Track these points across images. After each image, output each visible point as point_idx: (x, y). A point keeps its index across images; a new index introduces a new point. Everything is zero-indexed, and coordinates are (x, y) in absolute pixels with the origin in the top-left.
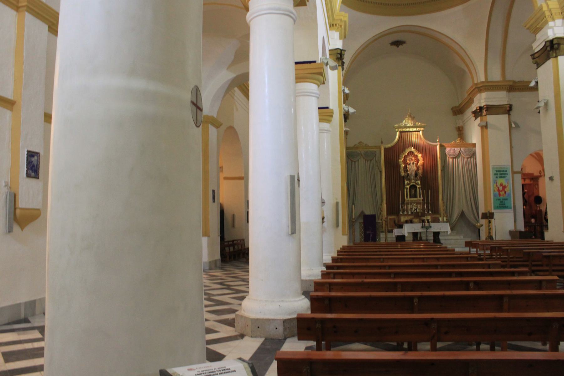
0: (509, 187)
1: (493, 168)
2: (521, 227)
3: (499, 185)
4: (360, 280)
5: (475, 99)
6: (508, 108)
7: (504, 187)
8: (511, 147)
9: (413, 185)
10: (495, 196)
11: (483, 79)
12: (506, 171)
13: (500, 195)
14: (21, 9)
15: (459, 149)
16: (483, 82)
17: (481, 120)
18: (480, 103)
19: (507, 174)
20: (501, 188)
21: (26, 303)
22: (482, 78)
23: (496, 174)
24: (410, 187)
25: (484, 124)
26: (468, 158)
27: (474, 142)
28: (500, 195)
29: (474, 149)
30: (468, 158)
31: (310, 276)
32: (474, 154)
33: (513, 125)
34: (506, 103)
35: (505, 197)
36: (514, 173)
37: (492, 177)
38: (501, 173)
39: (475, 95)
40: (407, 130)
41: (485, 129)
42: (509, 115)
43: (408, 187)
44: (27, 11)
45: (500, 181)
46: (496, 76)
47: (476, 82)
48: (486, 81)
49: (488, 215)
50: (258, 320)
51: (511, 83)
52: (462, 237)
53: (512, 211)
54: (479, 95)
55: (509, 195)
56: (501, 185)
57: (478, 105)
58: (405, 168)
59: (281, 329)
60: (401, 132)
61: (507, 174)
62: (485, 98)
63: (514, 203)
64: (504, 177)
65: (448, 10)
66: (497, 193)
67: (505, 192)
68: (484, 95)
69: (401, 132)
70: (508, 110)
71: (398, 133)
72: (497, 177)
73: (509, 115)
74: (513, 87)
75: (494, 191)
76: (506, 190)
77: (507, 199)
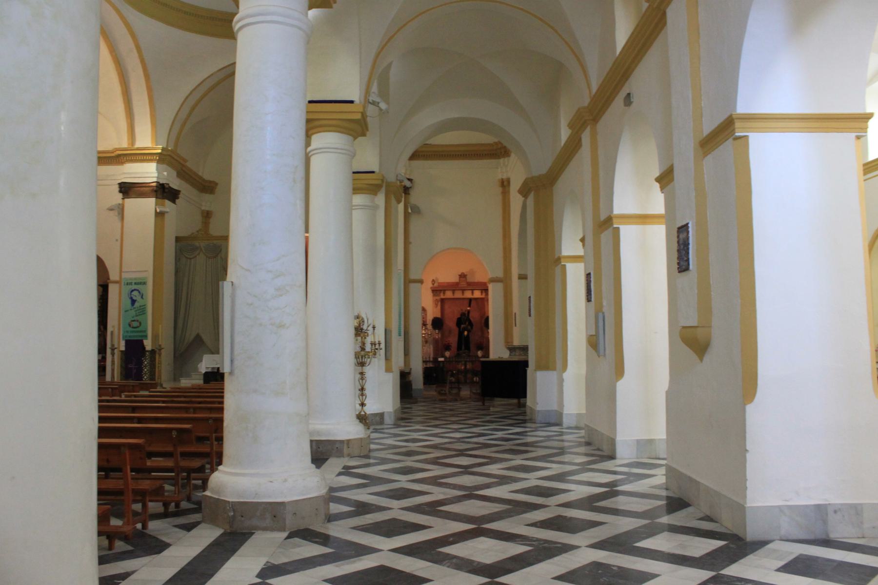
21: (434, 295)
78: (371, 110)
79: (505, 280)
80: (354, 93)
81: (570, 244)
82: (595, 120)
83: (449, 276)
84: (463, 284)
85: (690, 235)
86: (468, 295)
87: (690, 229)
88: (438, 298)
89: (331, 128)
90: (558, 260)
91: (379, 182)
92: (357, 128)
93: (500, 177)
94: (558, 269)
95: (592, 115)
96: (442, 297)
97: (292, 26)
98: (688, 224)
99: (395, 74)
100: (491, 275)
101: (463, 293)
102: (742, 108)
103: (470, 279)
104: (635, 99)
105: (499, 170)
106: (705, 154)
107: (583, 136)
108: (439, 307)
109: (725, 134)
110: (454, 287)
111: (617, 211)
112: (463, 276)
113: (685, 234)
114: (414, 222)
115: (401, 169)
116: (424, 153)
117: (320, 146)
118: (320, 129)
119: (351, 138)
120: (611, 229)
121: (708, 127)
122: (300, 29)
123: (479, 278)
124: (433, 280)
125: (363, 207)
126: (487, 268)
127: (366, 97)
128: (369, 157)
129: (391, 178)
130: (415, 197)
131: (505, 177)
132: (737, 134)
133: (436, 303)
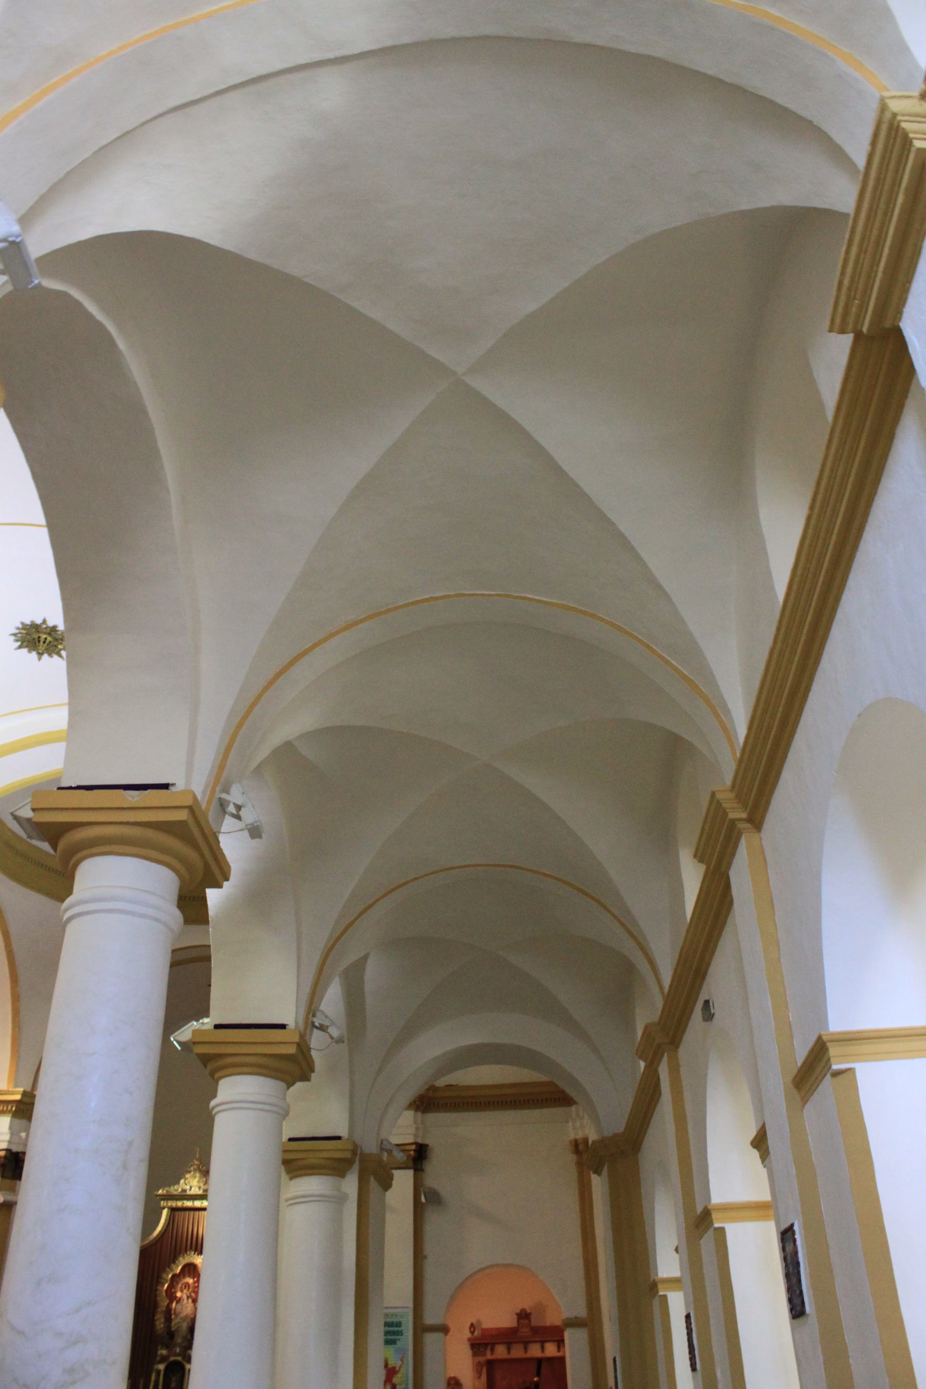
0: (403, 1371)
9: (176, 1363)
12: (399, 1324)
21: (475, 1354)
24: (166, 1369)
40: (189, 1204)
43: (161, 1367)
58: (168, 1312)
60: (173, 1210)
65: (594, 1189)
69: (173, 1210)
71: (165, 1212)
78: (317, 1040)
79: (590, 1322)
80: (286, 1011)
81: (668, 1263)
82: (675, 1041)
83: (499, 1317)
84: (525, 1332)
85: (799, 1243)
86: (535, 1351)
87: (797, 1236)
88: (482, 1359)
89: (245, 1069)
90: (653, 1287)
91: (348, 1155)
92: (293, 1067)
93: (572, 1136)
94: (656, 1302)
95: (668, 1036)
96: (489, 1356)
97: (157, 920)
98: (792, 1225)
99: (374, 975)
100: (567, 1313)
101: (526, 1349)
102: (836, 1024)
103: (535, 1322)
104: (716, 1010)
105: (570, 1124)
106: (805, 1100)
107: (660, 1069)
108: (484, 1377)
109: (816, 1068)
110: (508, 1337)
111: (717, 1198)
112: (523, 1316)
113: (792, 1245)
114: (434, 1222)
115: (403, 1129)
116: (427, 1102)
117: (230, 1098)
118: (231, 1070)
119: (282, 1085)
120: (711, 1232)
121: (801, 1055)
122: (157, 920)
123: (552, 1319)
124: (472, 1325)
125: (321, 1198)
126: (566, 1303)
127: (307, 1018)
128: (322, 1110)
129: (370, 1146)
130: (437, 1174)
131: (580, 1136)
132: (835, 1067)
133: (478, 1368)
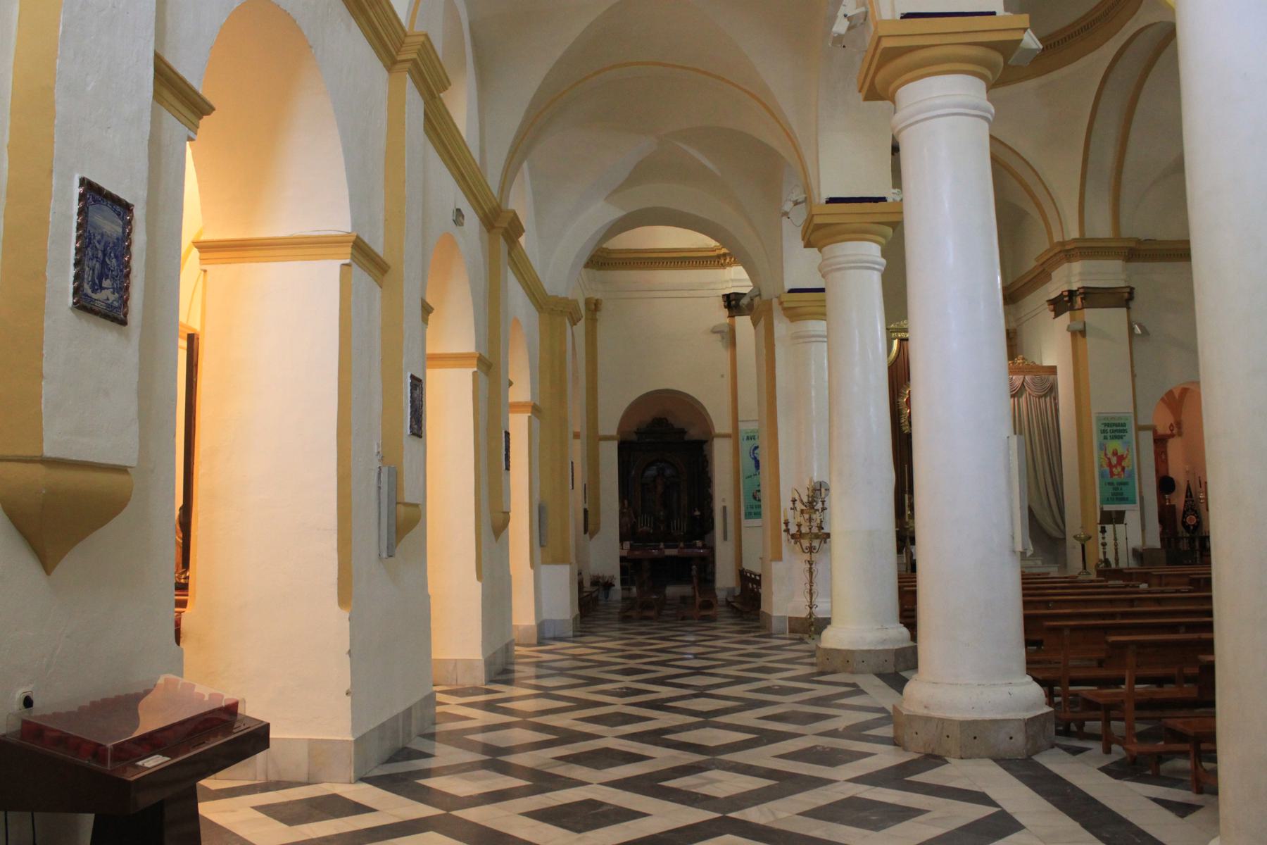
1: (1098, 419)
2: (1154, 541)
3: (1110, 455)
4: (1195, 636)
5: (1053, 274)
6: (1126, 295)
7: (1121, 458)
8: (1134, 376)
10: (1102, 475)
11: (1075, 234)
12: (1124, 425)
13: (1112, 474)
14: (398, 66)
15: (1021, 377)
16: (1075, 240)
17: (1072, 319)
18: (1069, 282)
19: (1125, 431)
20: (1114, 460)
22: (1073, 233)
23: (1103, 431)
25: (1080, 327)
26: (1040, 397)
27: (1048, 362)
28: (1112, 474)
29: (1051, 377)
30: (1040, 397)
31: (884, 641)
32: (1052, 390)
33: (1138, 330)
34: (1122, 284)
35: (1123, 478)
36: (1140, 428)
37: (1096, 438)
38: (1114, 429)
39: (1058, 264)
41: (1079, 336)
42: (1128, 308)
44: (410, 72)
45: (1114, 445)
46: (1101, 228)
47: (1057, 238)
48: (1082, 239)
49: (1114, 516)
50: (975, 722)
51: (1132, 245)
52: (1039, 563)
53: (1137, 507)
54: (1066, 265)
55: (1131, 475)
56: (1115, 453)
57: (1066, 288)
59: (1020, 739)
61: (1125, 431)
62: (1080, 274)
63: (1141, 492)
64: (1121, 437)
66: (1107, 469)
67: (1123, 469)
68: (1077, 267)
70: (1122, 298)
72: (1105, 438)
73: (1128, 308)
74: (1135, 252)
75: (1101, 466)
76: (1124, 464)
77: (1125, 484)
